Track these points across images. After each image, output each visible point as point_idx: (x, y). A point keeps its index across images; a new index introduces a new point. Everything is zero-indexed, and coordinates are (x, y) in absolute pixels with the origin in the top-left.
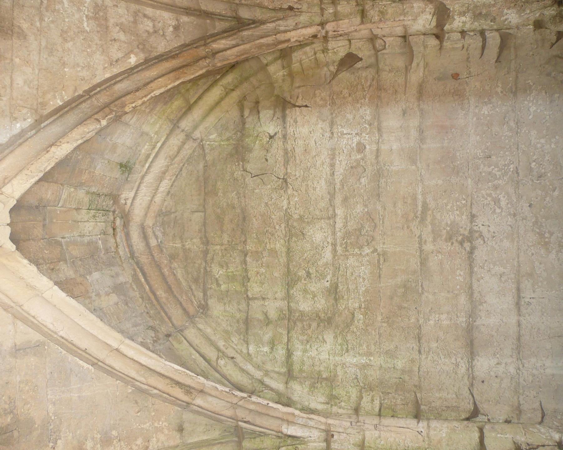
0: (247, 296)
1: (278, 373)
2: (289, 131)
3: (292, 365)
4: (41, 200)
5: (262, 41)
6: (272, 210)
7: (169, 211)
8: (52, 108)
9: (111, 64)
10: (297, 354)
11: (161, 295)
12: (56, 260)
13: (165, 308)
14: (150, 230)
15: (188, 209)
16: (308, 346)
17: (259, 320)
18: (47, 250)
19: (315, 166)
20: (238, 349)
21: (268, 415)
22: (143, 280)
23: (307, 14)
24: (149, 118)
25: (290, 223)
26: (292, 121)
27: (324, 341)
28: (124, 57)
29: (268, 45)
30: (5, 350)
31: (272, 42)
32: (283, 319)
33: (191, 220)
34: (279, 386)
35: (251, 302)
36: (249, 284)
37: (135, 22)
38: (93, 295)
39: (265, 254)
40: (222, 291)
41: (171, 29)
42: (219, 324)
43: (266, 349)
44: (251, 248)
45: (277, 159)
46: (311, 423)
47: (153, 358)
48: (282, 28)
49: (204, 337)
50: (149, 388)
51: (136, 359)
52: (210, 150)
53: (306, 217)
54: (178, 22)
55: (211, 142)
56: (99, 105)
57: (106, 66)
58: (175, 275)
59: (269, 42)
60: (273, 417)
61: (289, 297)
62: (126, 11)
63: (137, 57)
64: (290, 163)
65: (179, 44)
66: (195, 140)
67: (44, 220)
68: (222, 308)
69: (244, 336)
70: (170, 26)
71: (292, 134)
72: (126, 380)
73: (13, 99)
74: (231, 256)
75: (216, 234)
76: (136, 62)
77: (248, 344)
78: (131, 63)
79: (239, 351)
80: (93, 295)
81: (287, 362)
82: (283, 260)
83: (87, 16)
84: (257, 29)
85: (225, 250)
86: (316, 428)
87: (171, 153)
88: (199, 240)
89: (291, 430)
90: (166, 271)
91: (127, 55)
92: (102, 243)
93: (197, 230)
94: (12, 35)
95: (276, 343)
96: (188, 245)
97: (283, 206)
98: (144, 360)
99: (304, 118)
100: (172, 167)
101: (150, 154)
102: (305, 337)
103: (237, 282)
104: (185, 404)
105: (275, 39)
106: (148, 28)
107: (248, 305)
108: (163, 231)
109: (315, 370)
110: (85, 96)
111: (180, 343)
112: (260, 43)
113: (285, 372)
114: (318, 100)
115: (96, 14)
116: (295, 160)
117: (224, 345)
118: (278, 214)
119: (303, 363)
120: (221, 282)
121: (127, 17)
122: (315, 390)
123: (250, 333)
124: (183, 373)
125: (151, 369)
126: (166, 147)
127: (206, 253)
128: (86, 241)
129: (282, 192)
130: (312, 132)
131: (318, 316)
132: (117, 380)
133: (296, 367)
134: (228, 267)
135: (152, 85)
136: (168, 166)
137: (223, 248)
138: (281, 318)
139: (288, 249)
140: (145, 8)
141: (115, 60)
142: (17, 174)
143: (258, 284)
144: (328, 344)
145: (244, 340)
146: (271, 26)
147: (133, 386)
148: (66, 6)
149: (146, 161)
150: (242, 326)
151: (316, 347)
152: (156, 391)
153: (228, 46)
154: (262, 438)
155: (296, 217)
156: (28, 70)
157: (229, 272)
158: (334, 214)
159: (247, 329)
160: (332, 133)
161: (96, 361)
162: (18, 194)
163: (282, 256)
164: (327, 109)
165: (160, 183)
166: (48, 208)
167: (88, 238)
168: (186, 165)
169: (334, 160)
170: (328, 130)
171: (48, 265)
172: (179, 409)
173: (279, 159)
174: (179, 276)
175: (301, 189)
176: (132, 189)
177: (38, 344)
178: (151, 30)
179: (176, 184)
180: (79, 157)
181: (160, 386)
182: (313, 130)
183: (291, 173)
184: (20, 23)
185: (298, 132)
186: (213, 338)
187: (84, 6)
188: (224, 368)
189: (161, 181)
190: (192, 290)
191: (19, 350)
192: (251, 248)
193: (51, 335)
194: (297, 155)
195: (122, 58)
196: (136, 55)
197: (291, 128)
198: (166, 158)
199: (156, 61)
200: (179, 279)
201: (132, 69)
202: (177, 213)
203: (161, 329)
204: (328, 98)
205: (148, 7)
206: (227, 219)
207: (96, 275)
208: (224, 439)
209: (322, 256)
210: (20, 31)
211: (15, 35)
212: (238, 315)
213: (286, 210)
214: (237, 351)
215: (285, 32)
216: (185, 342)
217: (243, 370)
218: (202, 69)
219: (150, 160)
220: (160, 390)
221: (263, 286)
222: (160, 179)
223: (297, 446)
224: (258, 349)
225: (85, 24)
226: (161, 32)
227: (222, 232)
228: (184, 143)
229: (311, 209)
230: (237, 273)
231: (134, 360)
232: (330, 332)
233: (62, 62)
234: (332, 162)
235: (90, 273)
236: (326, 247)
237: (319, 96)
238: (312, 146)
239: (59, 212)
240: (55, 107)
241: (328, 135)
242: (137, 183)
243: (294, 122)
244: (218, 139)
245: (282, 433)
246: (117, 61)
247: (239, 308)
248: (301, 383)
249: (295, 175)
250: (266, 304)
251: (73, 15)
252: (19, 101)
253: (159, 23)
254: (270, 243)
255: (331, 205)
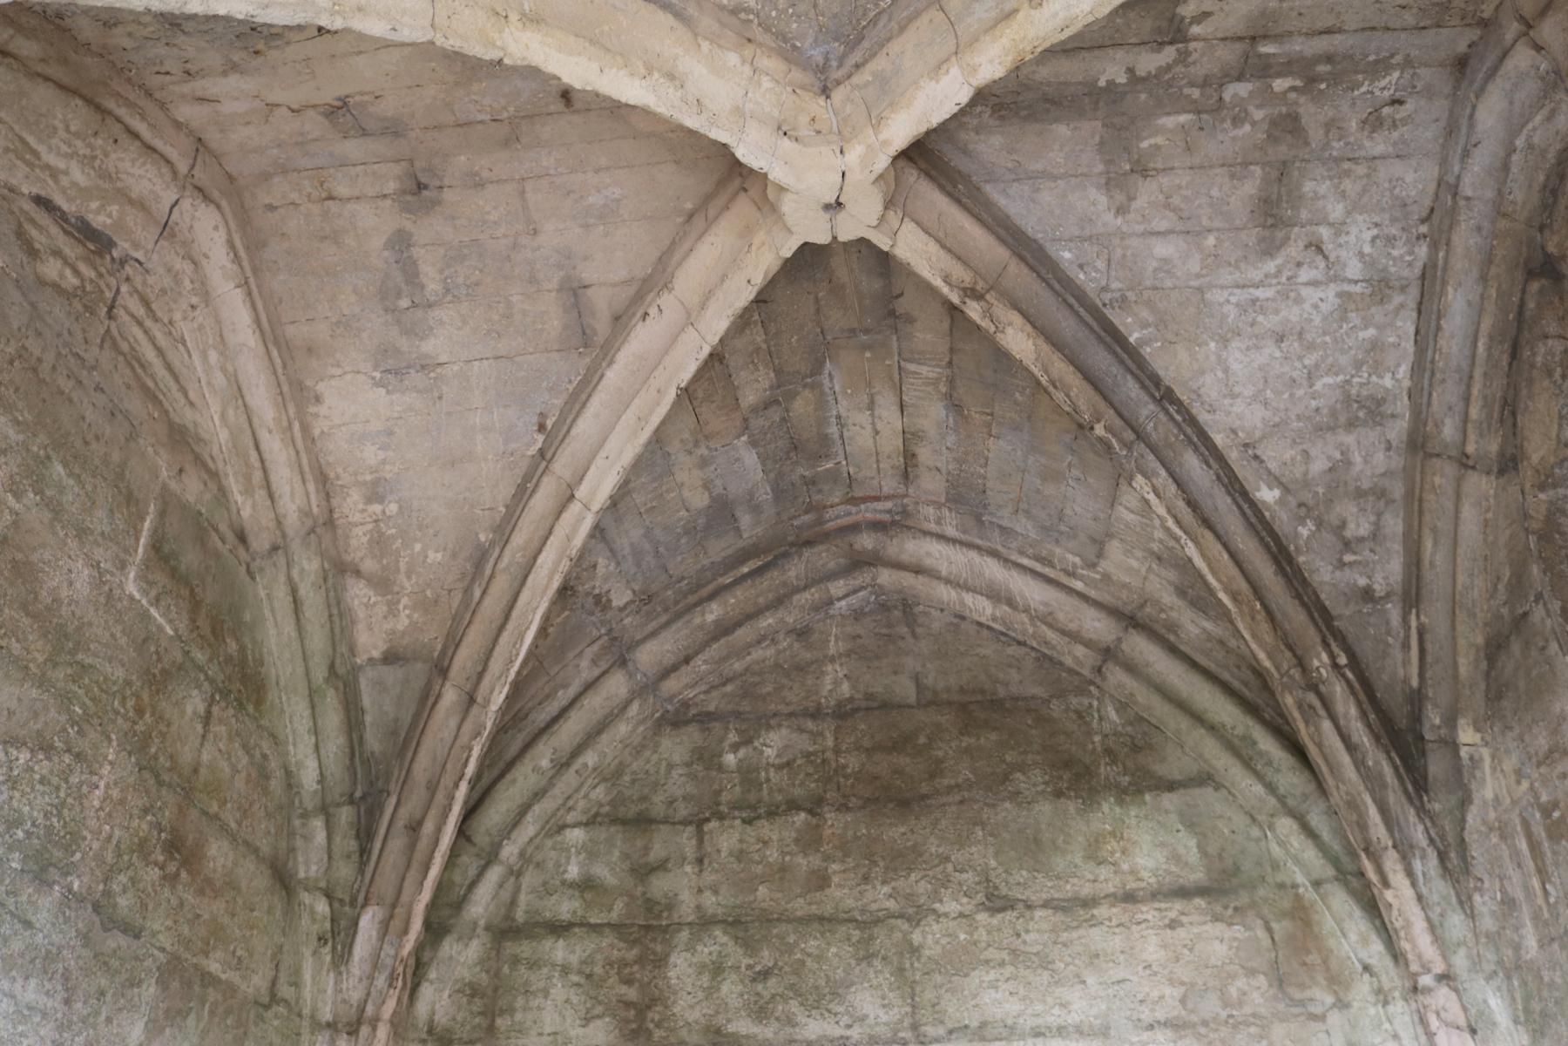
0: (708, 820)
1: (513, 903)
2: (1144, 909)
3: (531, 937)
4: (910, 320)
5: (1373, 813)
6: (930, 873)
7: (915, 621)
8: (1116, 322)
9: (1246, 445)
10: (560, 950)
11: (712, 613)
12: (777, 362)
13: (680, 624)
14: (868, 580)
15: (924, 666)
16: (575, 978)
17: (646, 849)
18: (798, 341)
19: (1056, 983)
20: (576, 802)
21: (408, 867)
22: (745, 570)
23: (1470, 935)
24: (1139, 554)
25: (899, 921)
26: (1173, 914)
27: (587, 1020)
28: (1270, 473)
29: (1363, 826)
30: (574, 268)
31: (1375, 839)
32: (649, 910)
33: (895, 673)
34: (481, 905)
35: (691, 829)
36: (738, 822)
37: (1360, 494)
38: (703, 451)
39: (815, 861)
40: (720, 756)
41: (1362, 582)
42: (638, 752)
43: (573, 871)
44: (830, 823)
45: (1067, 882)
46: (381, 981)
47: (551, 578)
48: (1417, 865)
49: (606, 717)
50: (486, 578)
51: (549, 542)
52: (1077, 712)
53: (916, 965)
54: (1381, 598)
55: (1099, 711)
56: (1141, 420)
57: (1240, 434)
58: (759, 642)
59: (1372, 831)
60: (403, 879)
61: (703, 925)
62: (1382, 470)
63: (1276, 503)
64: (1060, 917)
65: (1327, 603)
66: (1099, 671)
67: (867, 331)
68: (677, 758)
69: (607, 815)
70: (1370, 578)
71: (1140, 917)
72: (505, 528)
73: (1122, 239)
74: (808, 775)
75: (864, 736)
76: (1264, 503)
77: (587, 824)
78: (1259, 490)
79: (571, 803)
80: (703, 451)
81: (537, 924)
82: (800, 907)
83: (1348, 382)
84: (1403, 799)
85: (824, 761)
86: (368, 994)
87: (1061, 616)
88: (847, 696)
89: (368, 922)
90: (767, 621)
91: (1275, 481)
92: (827, 470)
93: (871, 690)
94: (1264, 227)
95: (589, 896)
96: (834, 671)
97: (941, 901)
98: (547, 558)
99: (1185, 946)
100: (1026, 620)
101: (1051, 565)
102: (598, 970)
103: (743, 792)
104: (446, 663)
105: (1383, 845)
106: (1352, 526)
107: (685, 822)
108: (867, 610)
109: (515, 997)
110: (1159, 390)
111: (594, 662)
112: (1365, 804)
113: (513, 920)
114: (1241, 983)
115: (1357, 402)
116: (1068, 928)
117: (586, 765)
118: (921, 891)
119: (534, 965)
120: (742, 753)
121: (1369, 474)
122: (465, 999)
123: (613, 829)
124: (514, 652)
125: (526, 577)
126: (1075, 601)
127: (816, 714)
128: (830, 431)
129: (980, 897)
130: (1148, 972)
131: (654, 1001)
132: (507, 507)
133: (524, 949)
134: (779, 768)
135: (1209, 536)
136: (1027, 610)
137: (829, 754)
138: (650, 904)
139: (830, 920)
140: (1401, 514)
141: (1259, 452)
142: (950, 251)
143: (738, 846)
144: (581, 1031)
145: (597, 814)
146: (1419, 835)
147: (493, 543)
148: (1361, 335)
149: (1037, 558)
150: (632, 810)
151: (575, 999)
152: (477, 593)
153: (1342, 722)
154: (355, 857)
155: (916, 937)
156: (1194, 266)
157: (767, 773)
158: (927, 1040)
159: (624, 822)
160: (1151, 1027)
161: (549, 456)
162: (902, 252)
163: (810, 904)
164: (1219, 1010)
165: (982, 594)
166: (895, 338)
167: (836, 436)
168: (1033, 654)
169: (1077, 1036)
170: (1160, 1015)
171: (764, 346)
172: (436, 654)
173: (1068, 887)
174: (757, 654)
175: (991, 949)
176: (964, 532)
177: (588, 331)
178: (1348, 534)
179: (985, 632)
180: (1017, 395)
181: (487, 602)
182: (1155, 974)
183: (1032, 919)
184: (1296, 241)
185: (1145, 933)
186: (605, 738)
187: (1370, 375)
188: (530, 767)
189: (988, 597)
190: (724, 684)
191: (576, 295)
192: (830, 823)
193: (606, 355)
194: (1081, 932)
195: (1267, 468)
196: (1281, 502)
197: (1156, 913)
198: (1046, 604)
199: (1274, 549)
200: (749, 654)
201: (1245, 494)
202: (912, 640)
203: (627, 616)
204: (1247, 1010)
205: (1404, 520)
206: (903, 761)
207: (750, 459)
208: (363, 763)
209: (813, 1012)
210: (1278, 243)
211: (1267, 233)
212: (659, 799)
213: (934, 911)
214: (569, 798)
215: (1410, 873)
216: (597, 672)
217: (524, 810)
218: (1270, 656)
219: (1038, 567)
220: (479, 603)
221: (732, 859)
222: (995, 594)
223: (330, 944)
224: (573, 850)
225: (1329, 380)
226: (1348, 558)
227: (869, 751)
228: (1088, 644)
229: (938, 978)
230: (765, 792)
231: (547, 538)
232: (612, 1035)
233: (1229, 335)
234: (1071, 1029)
235: (753, 443)
236: (837, 1023)
237: (1249, 985)
238: (1111, 972)
239: (887, 362)
240: (1122, 328)
241: (1146, 1015)
242: (979, 542)
243: (1172, 921)
244: (1106, 727)
245: (364, 906)
246: (1256, 457)
247: (676, 800)
248: (482, 962)
249: (1027, 931)
250: (688, 869)
251: (1343, 352)
252: (1119, 252)
253: (1372, 551)
254: (844, 871)
255: (951, 1032)
